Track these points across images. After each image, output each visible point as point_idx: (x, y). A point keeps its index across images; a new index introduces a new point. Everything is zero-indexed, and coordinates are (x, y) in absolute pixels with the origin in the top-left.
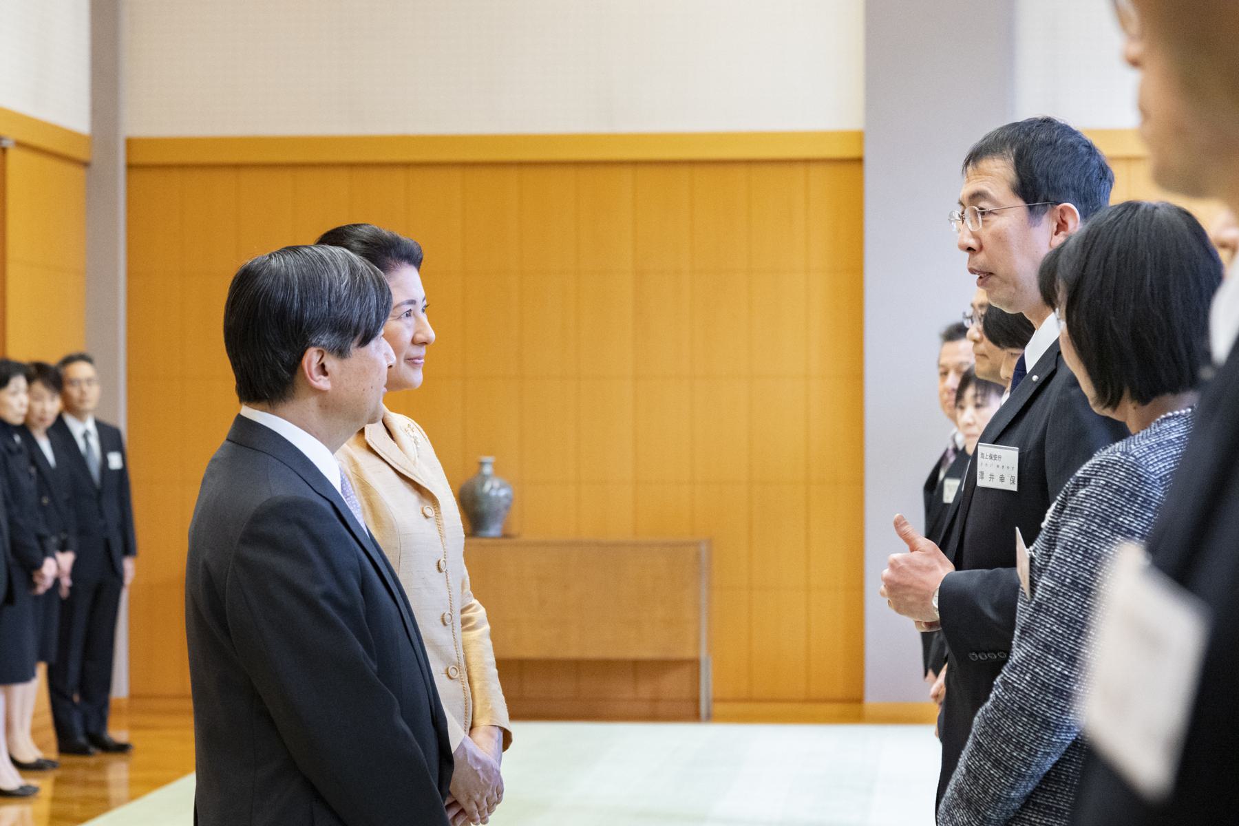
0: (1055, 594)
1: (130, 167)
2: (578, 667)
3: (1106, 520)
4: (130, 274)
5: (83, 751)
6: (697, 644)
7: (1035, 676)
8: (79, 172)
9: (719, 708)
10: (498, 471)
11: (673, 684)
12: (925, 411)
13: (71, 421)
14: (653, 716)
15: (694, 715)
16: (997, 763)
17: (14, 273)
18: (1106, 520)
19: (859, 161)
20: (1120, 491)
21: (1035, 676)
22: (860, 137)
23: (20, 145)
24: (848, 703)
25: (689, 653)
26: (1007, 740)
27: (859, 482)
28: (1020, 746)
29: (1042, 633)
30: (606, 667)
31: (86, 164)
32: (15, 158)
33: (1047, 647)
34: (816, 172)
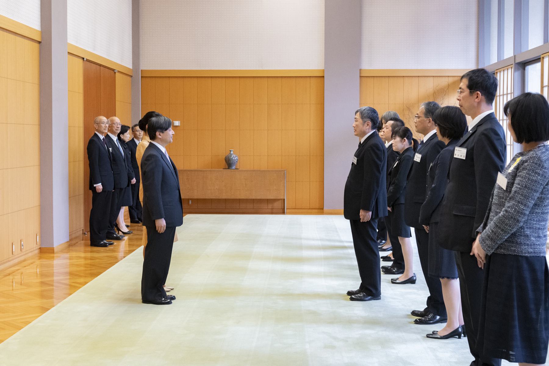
0: (520, 189)
1: (142, 77)
2: (253, 201)
3: (533, 171)
4: (142, 104)
5: (137, 222)
6: (284, 195)
7: (515, 209)
8: (129, 78)
9: (288, 211)
10: (234, 153)
11: (277, 205)
12: (119, 132)
13: (135, 140)
14: (272, 213)
15: (283, 213)
16: (502, 230)
17: (117, 104)
18: (533, 171)
19: (323, 77)
20: (536, 164)
21: (515, 209)
22: (323, 71)
23: (119, 71)
24: (320, 210)
25: (282, 198)
26: (506, 225)
27: (323, 156)
28: (510, 226)
29: (518, 199)
30: (260, 201)
31: (132, 76)
32: (117, 75)
33: (519, 202)
34: (312, 79)
